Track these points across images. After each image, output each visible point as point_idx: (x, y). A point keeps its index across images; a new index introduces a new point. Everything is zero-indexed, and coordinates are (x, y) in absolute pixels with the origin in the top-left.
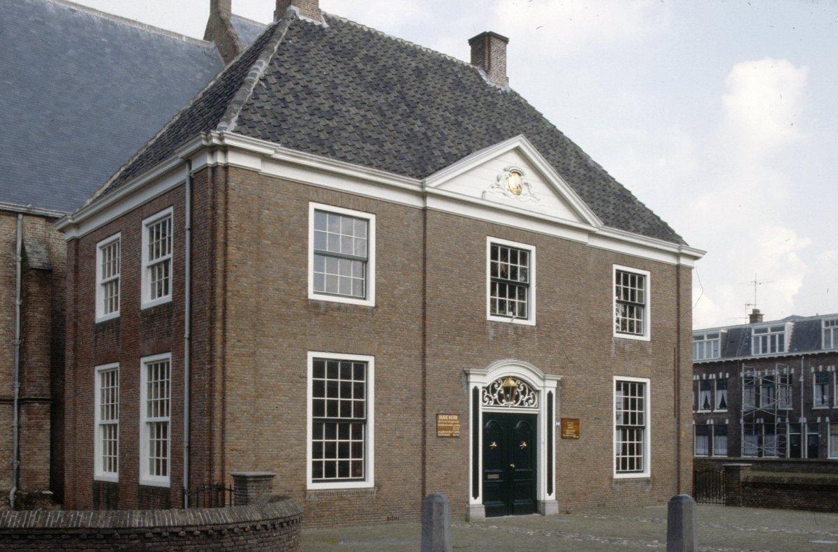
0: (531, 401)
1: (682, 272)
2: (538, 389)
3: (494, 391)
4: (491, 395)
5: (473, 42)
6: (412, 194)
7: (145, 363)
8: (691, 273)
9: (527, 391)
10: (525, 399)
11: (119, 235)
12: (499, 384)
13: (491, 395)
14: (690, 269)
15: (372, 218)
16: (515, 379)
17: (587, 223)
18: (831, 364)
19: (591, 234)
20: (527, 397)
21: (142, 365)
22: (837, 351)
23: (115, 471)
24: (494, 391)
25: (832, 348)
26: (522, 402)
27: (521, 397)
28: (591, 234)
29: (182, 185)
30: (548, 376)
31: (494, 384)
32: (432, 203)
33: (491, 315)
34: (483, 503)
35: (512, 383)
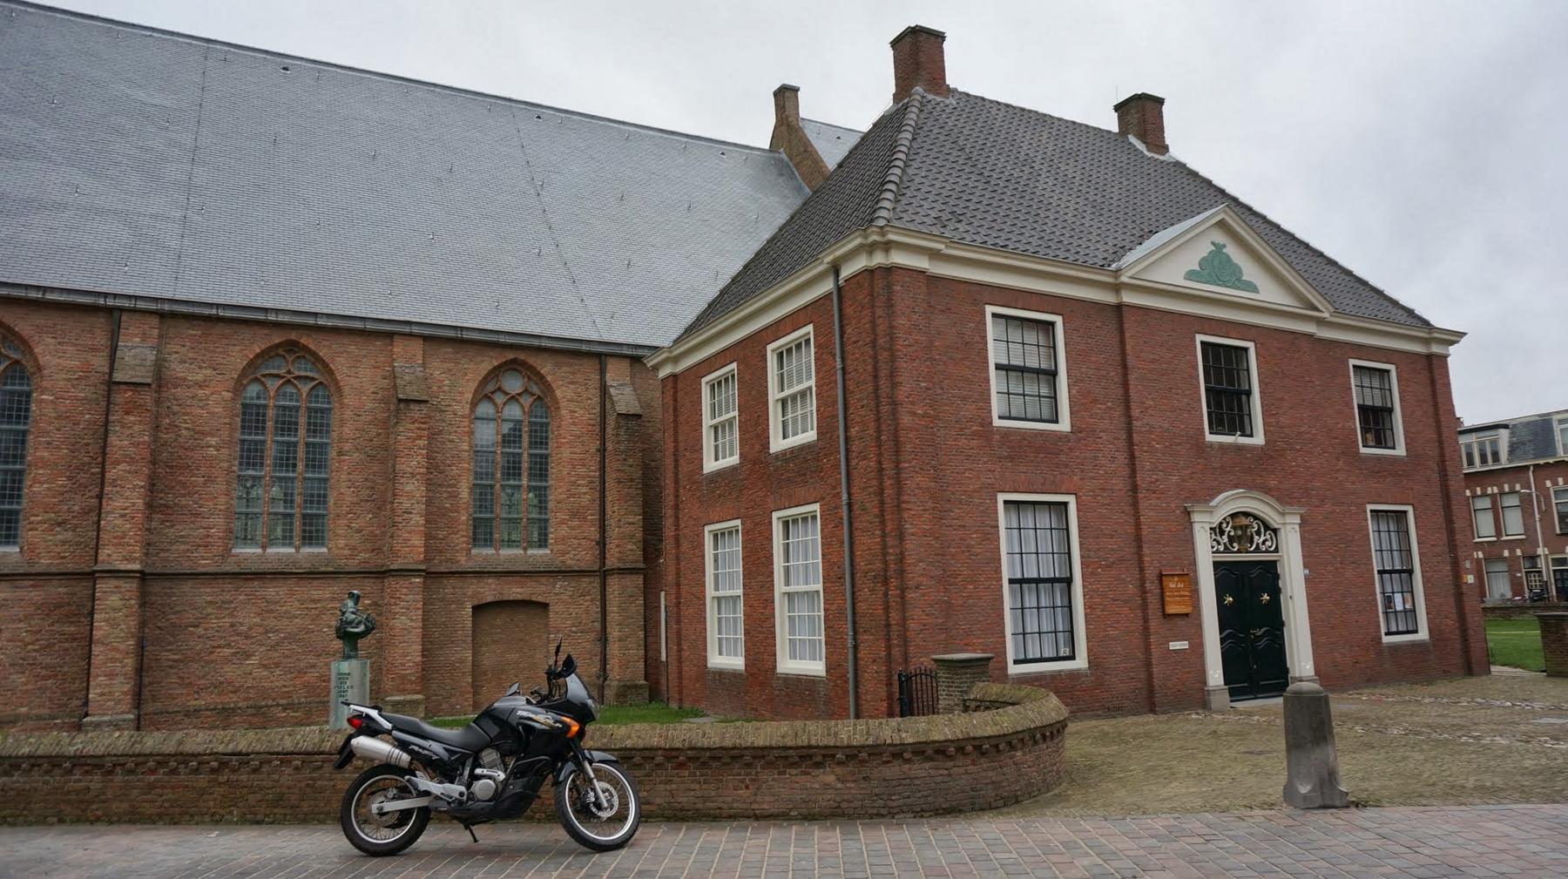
0: (1269, 543)
1: (1435, 361)
2: (1276, 526)
3: (1222, 533)
4: (1219, 538)
5: (1117, 108)
6: (1098, 287)
7: (779, 518)
8: (1446, 363)
9: (1262, 530)
10: (1261, 540)
11: (734, 366)
12: (1228, 523)
13: (1219, 538)
14: (1445, 357)
15: (1058, 320)
16: (1246, 514)
17: (1317, 309)
18: (1492, 486)
19: (1321, 322)
20: (1263, 538)
21: (775, 522)
22: (1566, 459)
23: (820, 659)
24: (1222, 533)
25: (1561, 455)
26: (1258, 544)
27: (1256, 537)
28: (1321, 322)
29: (828, 296)
30: (1288, 509)
31: (1221, 523)
32: (1128, 298)
33: (1211, 433)
34: (1226, 683)
35: (1244, 521)
